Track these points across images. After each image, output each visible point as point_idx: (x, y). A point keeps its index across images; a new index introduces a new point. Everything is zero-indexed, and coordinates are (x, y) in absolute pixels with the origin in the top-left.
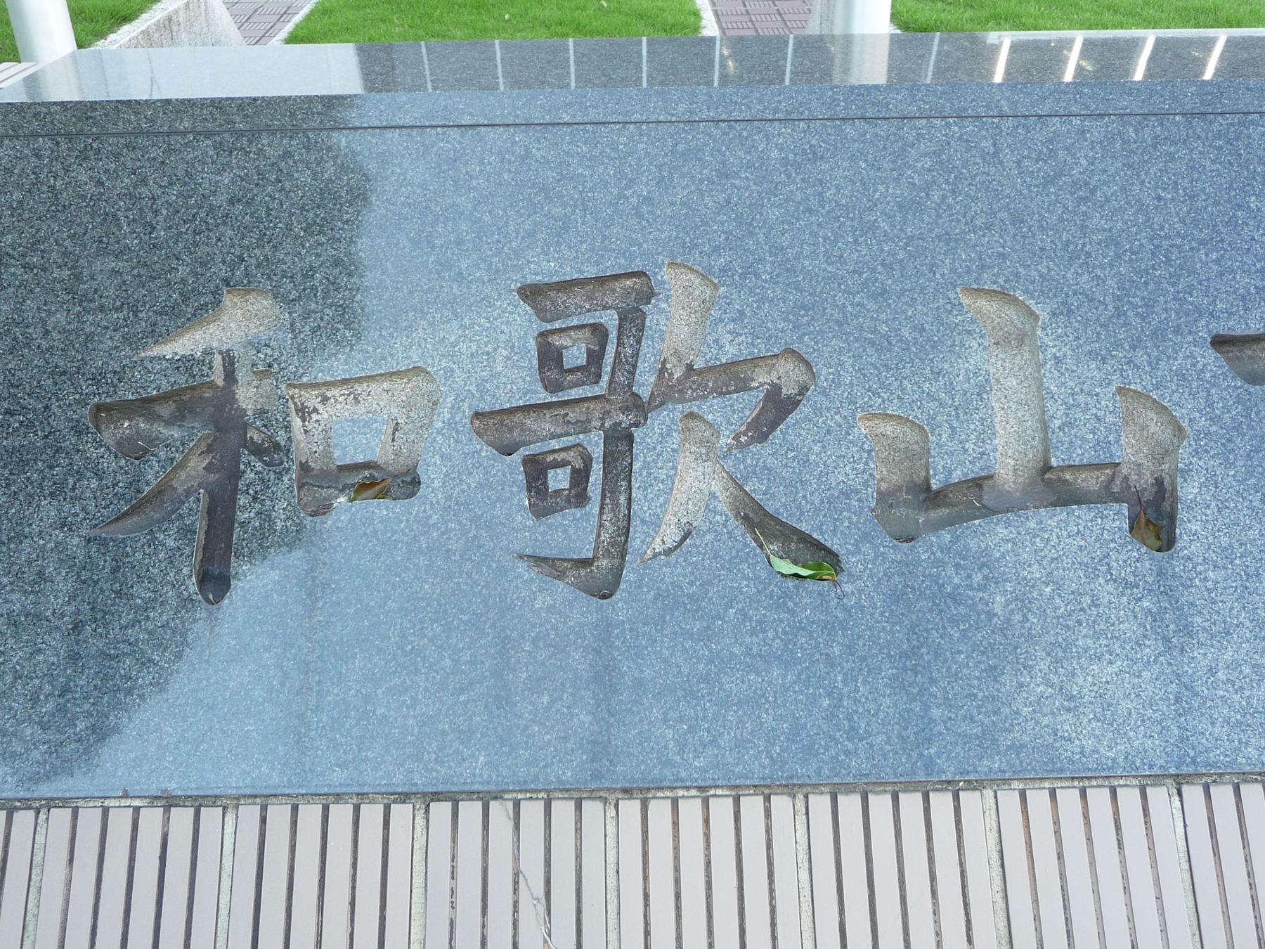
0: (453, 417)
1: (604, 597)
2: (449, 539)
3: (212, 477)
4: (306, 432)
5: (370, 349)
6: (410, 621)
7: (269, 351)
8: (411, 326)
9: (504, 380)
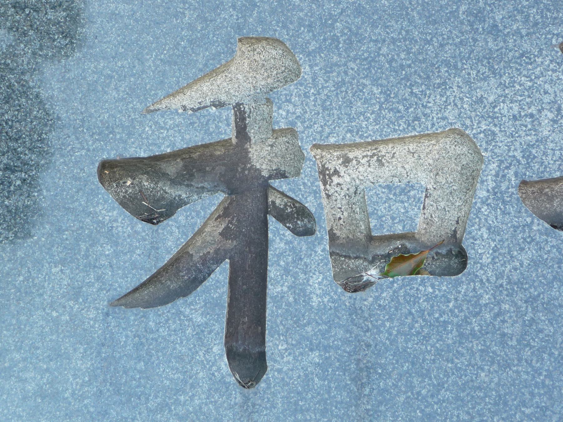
0: (498, 186)
1: (149, 221)
2: (504, 321)
3: (230, 244)
4: (328, 196)
5: (401, 107)
6: (468, 413)
7: (291, 108)
8: (445, 83)
9: (551, 145)
